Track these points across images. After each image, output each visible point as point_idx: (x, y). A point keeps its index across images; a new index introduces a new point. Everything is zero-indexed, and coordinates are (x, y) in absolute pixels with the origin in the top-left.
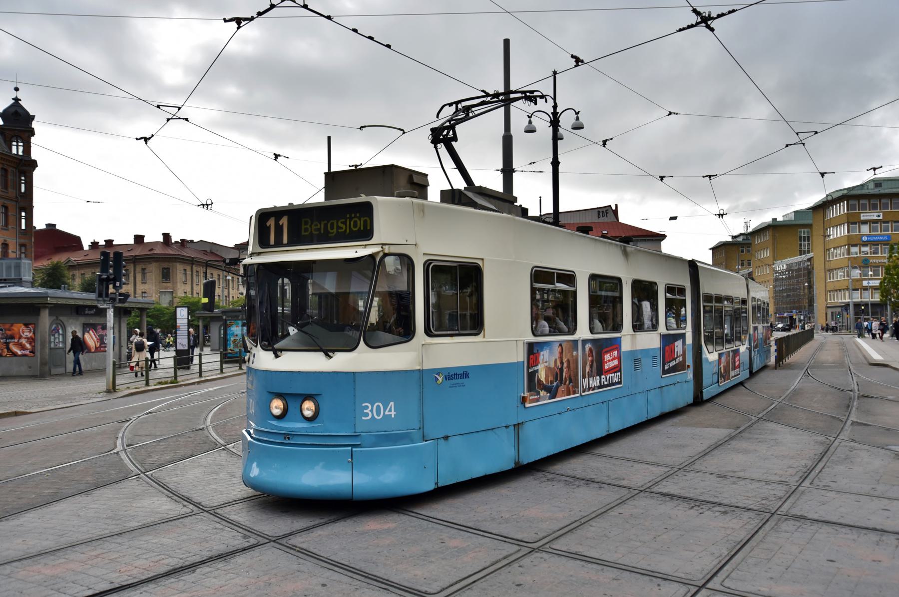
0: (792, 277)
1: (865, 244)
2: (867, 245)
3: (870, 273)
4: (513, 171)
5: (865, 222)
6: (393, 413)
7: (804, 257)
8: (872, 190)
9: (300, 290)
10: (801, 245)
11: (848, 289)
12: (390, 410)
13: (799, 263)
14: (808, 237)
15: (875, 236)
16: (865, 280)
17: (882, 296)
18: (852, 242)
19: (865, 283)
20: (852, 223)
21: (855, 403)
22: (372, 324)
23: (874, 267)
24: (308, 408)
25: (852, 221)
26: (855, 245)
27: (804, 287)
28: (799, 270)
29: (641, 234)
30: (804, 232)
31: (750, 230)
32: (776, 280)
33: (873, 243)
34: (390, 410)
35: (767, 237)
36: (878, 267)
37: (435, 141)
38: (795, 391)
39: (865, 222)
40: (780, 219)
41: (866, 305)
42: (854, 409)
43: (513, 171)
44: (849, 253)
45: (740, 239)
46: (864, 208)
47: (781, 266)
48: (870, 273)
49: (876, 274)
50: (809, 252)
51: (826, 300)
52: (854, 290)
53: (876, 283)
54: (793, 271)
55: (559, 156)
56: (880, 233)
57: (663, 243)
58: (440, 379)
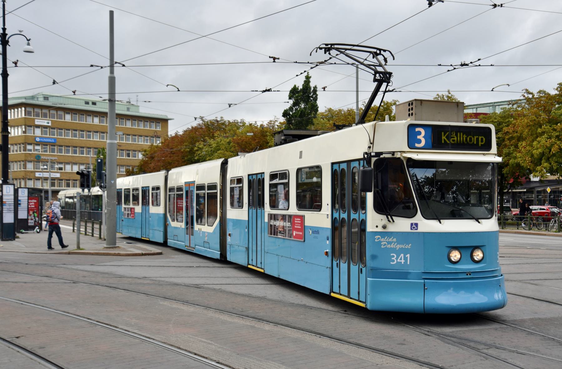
1: (38, 144)
2: (39, 145)
5: (38, 126)
8: (41, 101)
9: (257, 177)
15: (46, 138)
19: (37, 175)
24: (478, 255)
25: (29, 124)
26: (30, 144)
33: (44, 144)
34: (401, 259)
39: (38, 126)
44: (25, 150)
46: (38, 115)
55: (8, 69)
56: (49, 137)
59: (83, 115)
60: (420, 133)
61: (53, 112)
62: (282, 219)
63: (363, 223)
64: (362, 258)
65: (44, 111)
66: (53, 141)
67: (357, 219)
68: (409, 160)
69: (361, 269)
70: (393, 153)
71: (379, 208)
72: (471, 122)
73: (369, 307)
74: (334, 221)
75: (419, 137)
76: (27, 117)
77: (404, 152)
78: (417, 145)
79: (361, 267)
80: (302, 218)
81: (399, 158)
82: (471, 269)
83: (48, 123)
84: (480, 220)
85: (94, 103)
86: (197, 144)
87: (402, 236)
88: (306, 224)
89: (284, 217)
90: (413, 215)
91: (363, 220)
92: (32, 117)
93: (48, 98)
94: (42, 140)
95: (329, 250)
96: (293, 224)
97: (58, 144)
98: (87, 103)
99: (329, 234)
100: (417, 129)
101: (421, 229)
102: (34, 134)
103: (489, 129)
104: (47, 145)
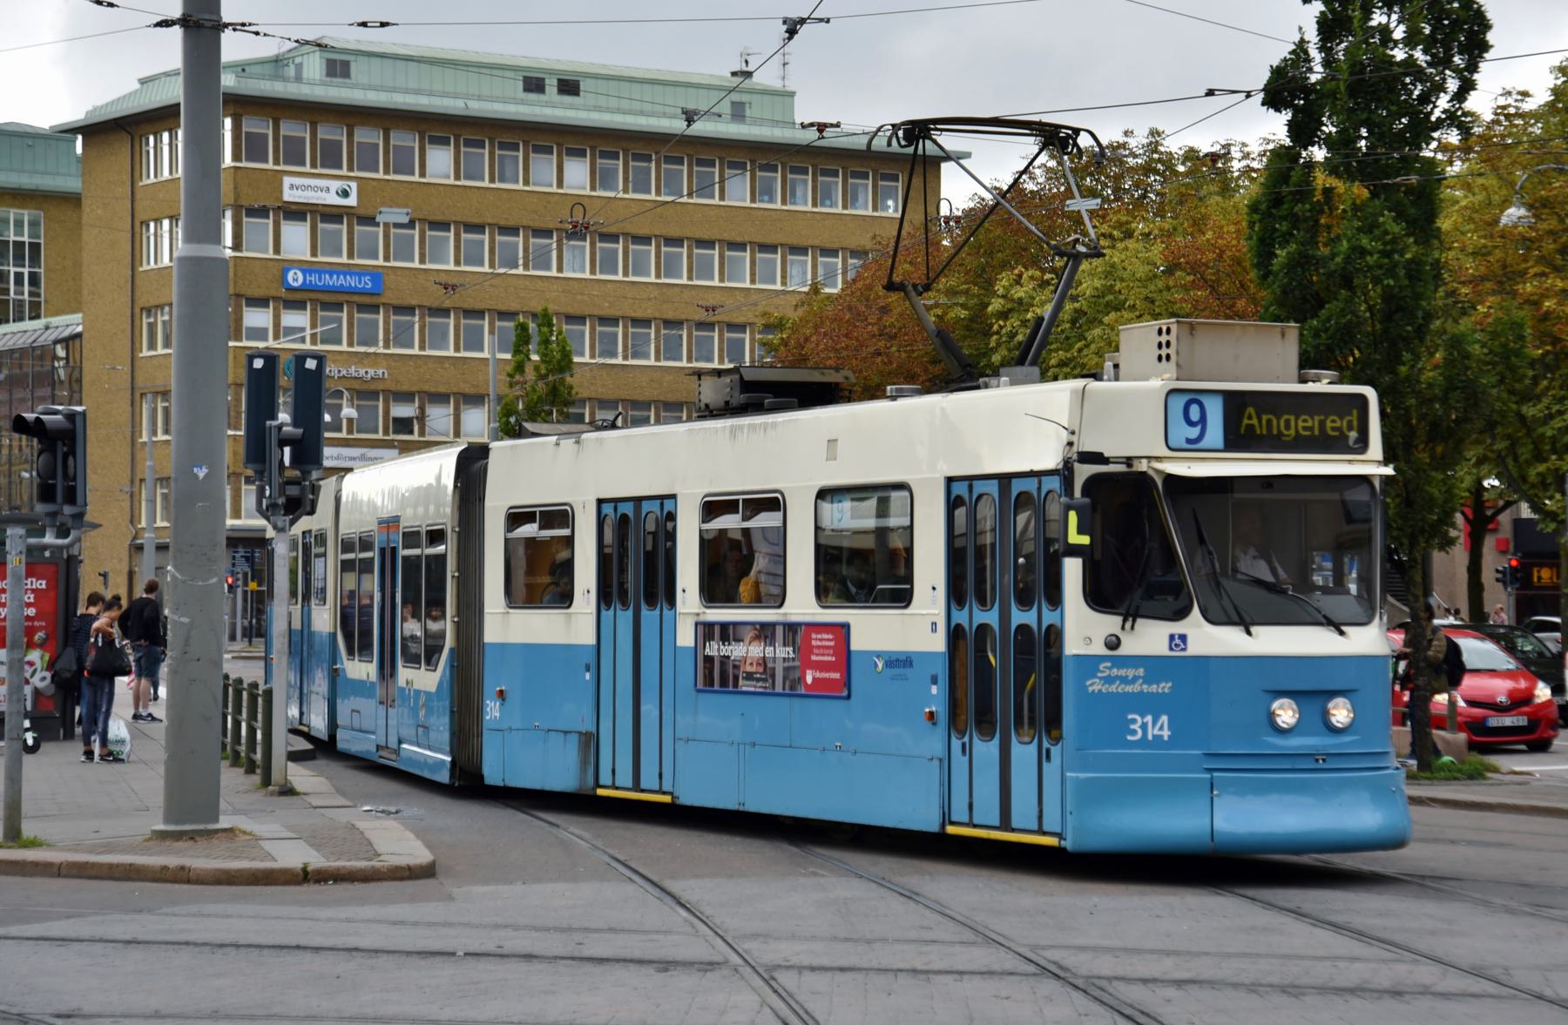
2: (298, 305)
4: (221, 27)
5: (296, 212)
6: (1166, 734)
8: (313, 84)
12: (1161, 728)
14: (35, 248)
15: (334, 269)
20: (252, 212)
26: (260, 302)
34: (1161, 728)
39: (296, 212)
43: (221, 27)
51: (134, 519)
58: (880, 665)
59: (515, 147)
61: (367, 135)
62: (757, 638)
63: (1054, 636)
64: (1052, 723)
65: (325, 132)
66: (367, 283)
67: (1034, 626)
68: (1170, 479)
69: (1048, 751)
70: (1129, 461)
71: (1097, 598)
72: (1317, 380)
73: (1068, 844)
74: (955, 635)
76: (243, 164)
77: (1158, 459)
79: (1046, 744)
80: (843, 630)
81: (1144, 473)
82: (1308, 747)
83: (345, 194)
84: (1344, 628)
85: (569, 87)
86: (1003, 283)
87: (1152, 666)
88: (854, 647)
89: (765, 632)
90: (1181, 614)
91: (1050, 627)
92: (270, 165)
93: (346, 64)
94: (313, 278)
95: (940, 707)
96: (804, 651)
97: (389, 297)
98: (534, 85)
99: (942, 670)
101: (1194, 648)
102: (277, 250)
103: (1363, 400)
104: (338, 306)
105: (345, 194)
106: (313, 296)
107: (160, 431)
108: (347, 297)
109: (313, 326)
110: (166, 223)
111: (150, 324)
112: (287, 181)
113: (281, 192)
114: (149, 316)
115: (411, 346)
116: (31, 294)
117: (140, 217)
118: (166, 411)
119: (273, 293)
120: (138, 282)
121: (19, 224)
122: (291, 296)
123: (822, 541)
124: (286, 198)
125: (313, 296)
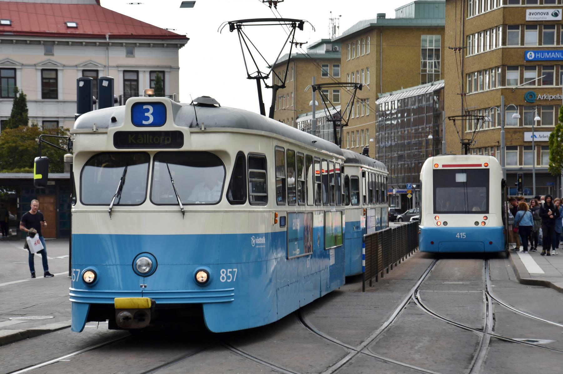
0: (409, 124)
2: (532, 68)
3: (537, 118)
5: (532, 25)
7: (429, 88)
10: (425, 65)
11: (498, 147)
13: (419, 98)
15: (549, 50)
16: (529, 130)
17: (553, 160)
18: (510, 61)
19: (528, 137)
20: (511, 27)
21: (484, 353)
22: (110, 327)
23: (545, 107)
26: (515, 68)
27: (427, 141)
28: (419, 110)
29: (148, 33)
30: (429, 41)
31: (339, 34)
32: (381, 128)
35: (367, 50)
36: (551, 107)
37: (232, 28)
38: (388, 330)
39: (532, 25)
40: (391, 15)
41: (527, 175)
42: (480, 362)
44: (503, 82)
45: (322, 51)
47: (389, 101)
48: (537, 118)
49: (546, 120)
50: (437, 78)
52: (509, 148)
53: (544, 136)
54: (409, 111)
57: (181, 51)
60: (148, 110)
75: (146, 114)
76: (508, 6)
78: (144, 122)
83: (556, 15)
92: (520, 5)
94: (539, 55)
100: (145, 107)
102: (522, 43)
104: (552, 67)
105: (556, 15)
106: (539, 63)
107: (496, 124)
108: (555, 63)
109: (539, 76)
110: (476, 35)
111: (469, 81)
112: (528, 11)
113: (525, 16)
114: (469, 77)
115: (552, 84)
116: (435, 71)
117: (467, 33)
118: (499, 114)
119: (520, 63)
120: (465, 62)
121: (431, 41)
122: (528, 64)
123: (484, 189)
124: (527, 19)
125: (539, 63)
